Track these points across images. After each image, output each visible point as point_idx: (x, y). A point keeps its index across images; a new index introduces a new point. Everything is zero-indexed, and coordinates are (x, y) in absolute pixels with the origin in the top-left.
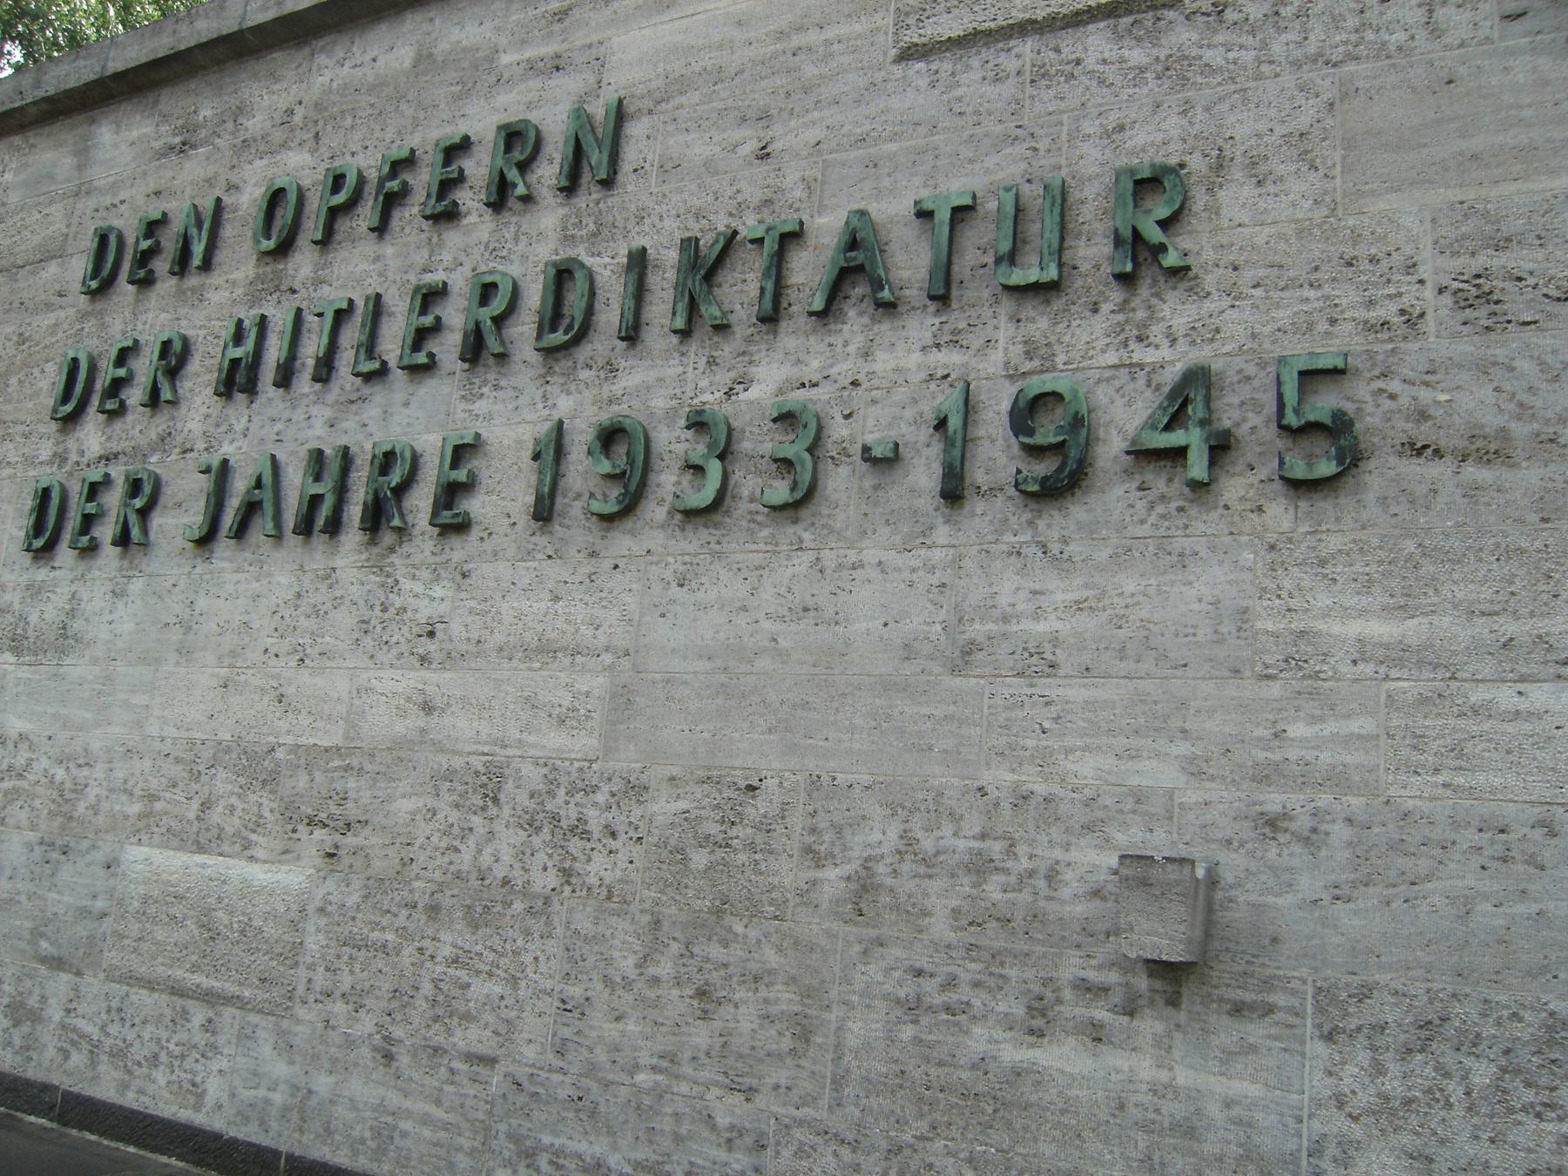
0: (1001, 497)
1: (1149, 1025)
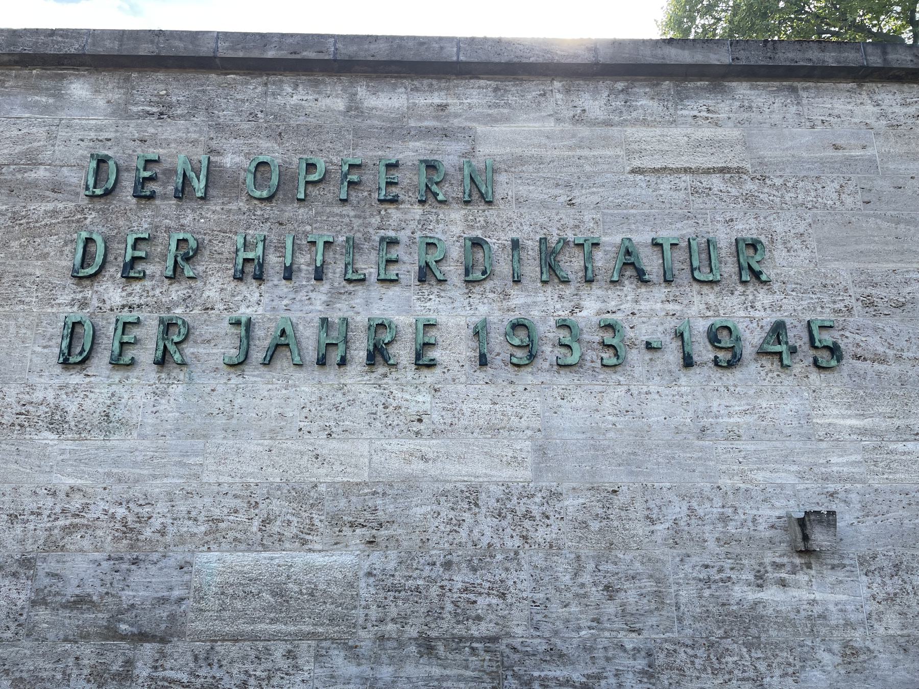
0: (706, 368)
1: (802, 577)
